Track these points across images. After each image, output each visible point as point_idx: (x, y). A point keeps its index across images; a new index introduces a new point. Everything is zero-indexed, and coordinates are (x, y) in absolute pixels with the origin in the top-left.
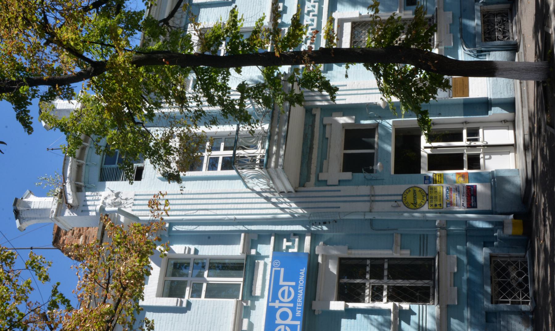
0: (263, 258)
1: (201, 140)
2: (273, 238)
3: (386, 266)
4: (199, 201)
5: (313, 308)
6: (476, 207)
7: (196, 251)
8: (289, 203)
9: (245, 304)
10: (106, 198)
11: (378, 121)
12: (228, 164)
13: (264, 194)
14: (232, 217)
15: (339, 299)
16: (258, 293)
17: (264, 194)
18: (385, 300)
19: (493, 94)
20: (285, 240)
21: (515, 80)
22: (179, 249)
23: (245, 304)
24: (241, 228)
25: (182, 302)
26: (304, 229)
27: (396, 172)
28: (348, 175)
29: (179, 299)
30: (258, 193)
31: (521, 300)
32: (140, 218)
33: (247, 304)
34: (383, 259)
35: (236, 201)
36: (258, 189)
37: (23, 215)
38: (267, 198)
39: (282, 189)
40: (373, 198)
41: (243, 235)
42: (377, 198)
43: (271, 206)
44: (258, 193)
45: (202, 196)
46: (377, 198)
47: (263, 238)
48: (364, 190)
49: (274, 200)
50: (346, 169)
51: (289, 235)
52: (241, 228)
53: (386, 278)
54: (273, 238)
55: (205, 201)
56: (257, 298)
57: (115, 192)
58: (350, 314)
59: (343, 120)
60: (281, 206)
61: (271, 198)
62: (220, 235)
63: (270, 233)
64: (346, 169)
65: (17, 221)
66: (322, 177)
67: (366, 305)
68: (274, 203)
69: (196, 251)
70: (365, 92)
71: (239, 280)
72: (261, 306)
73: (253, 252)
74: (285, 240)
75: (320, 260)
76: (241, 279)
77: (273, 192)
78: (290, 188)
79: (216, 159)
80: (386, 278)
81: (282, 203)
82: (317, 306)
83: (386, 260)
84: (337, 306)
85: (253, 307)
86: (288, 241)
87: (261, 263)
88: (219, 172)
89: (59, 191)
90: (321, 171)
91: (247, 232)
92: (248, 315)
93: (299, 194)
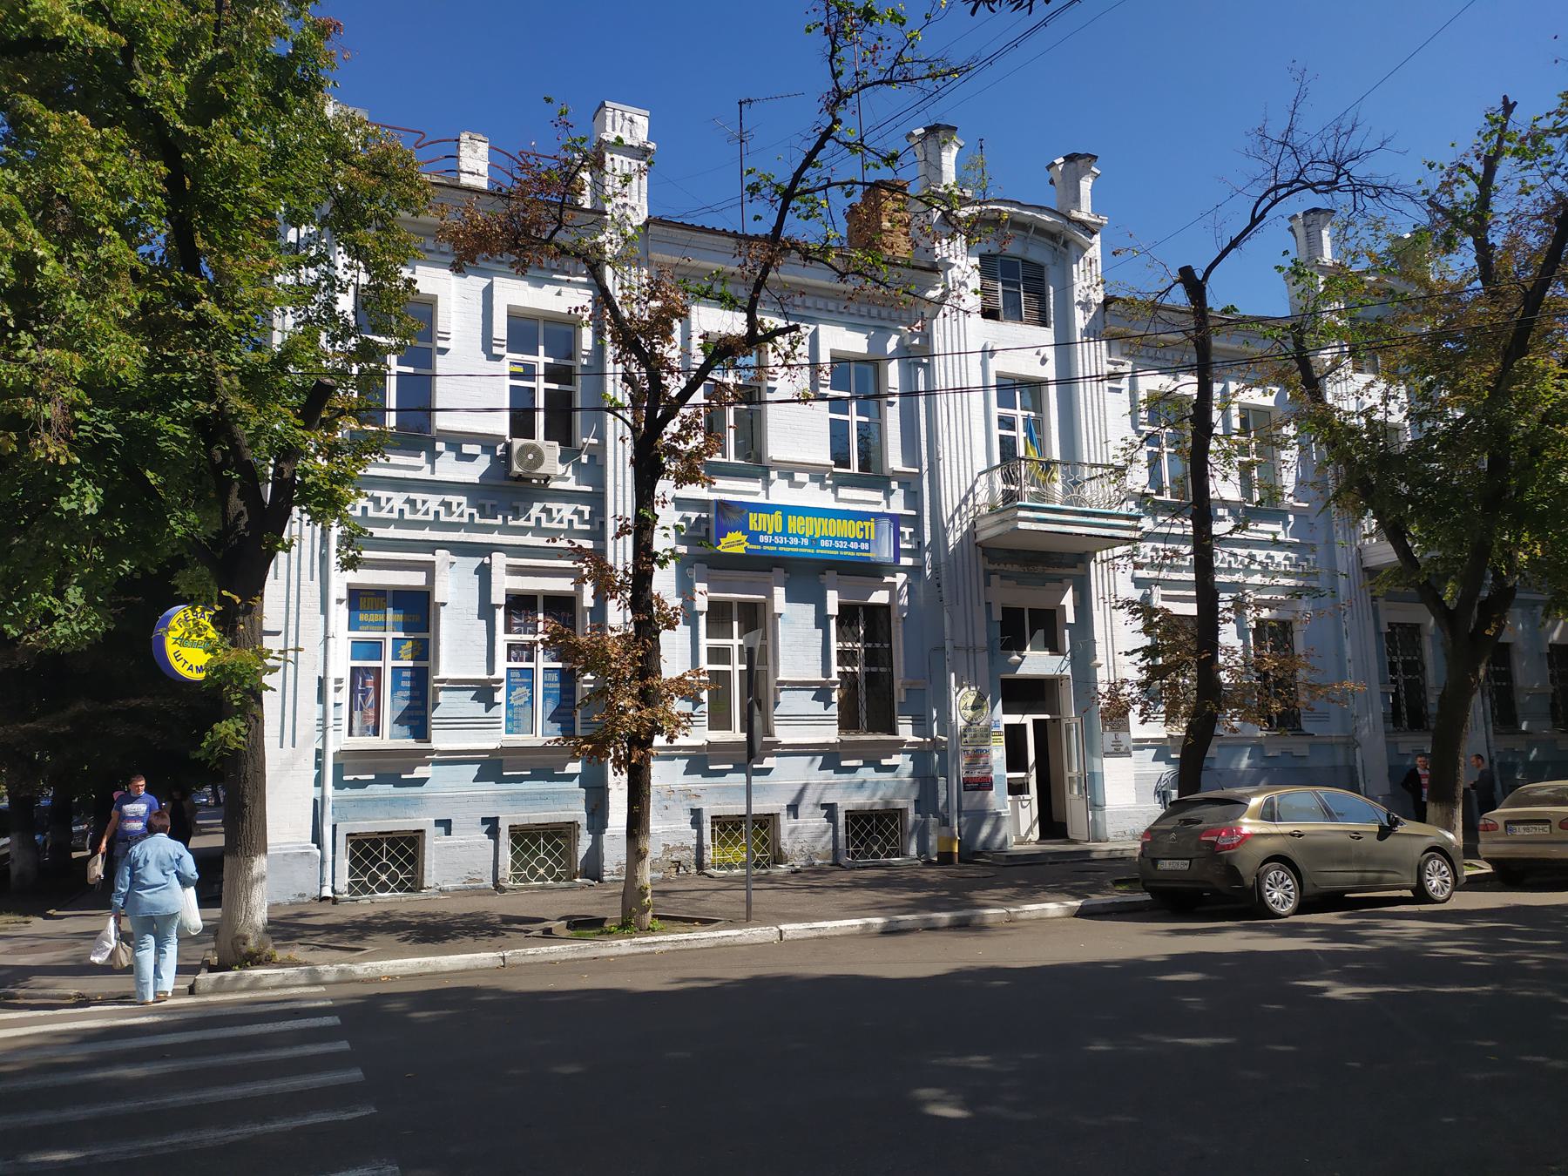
0: (887, 498)
1: (1037, 404)
2: (914, 513)
3: (882, 670)
4: (961, 465)
5: (827, 572)
6: (965, 790)
7: (892, 404)
8: (961, 529)
9: (827, 476)
10: (959, 267)
11: (1069, 655)
12: (1008, 445)
13: (971, 496)
14: (941, 456)
15: (841, 606)
16: (844, 492)
17: (971, 496)
18: (840, 669)
19: (1111, 814)
20: (912, 530)
21: (1213, 359)
22: (893, 375)
23: (827, 476)
24: (925, 467)
25: (826, 386)
26: (926, 543)
27: (1003, 680)
28: (998, 616)
29: (829, 383)
30: (972, 489)
31: (851, 849)
32: (935, 321)
33: (828, 479)
34: (891, 665)
35: (961, 460)
36: (978, 488)
37: (930, 141)
38: (965, 500)
39: (980, 524)
40: (971, 650)
41: (917, 470)
42: (971, 655)
43: (957, 504)
44: (972, 489)
45: (968, 448)
46: (971, 655)
47: (913, 498)
48: (982, 639)
49: (964, 509)
50: (1006, 611)
51: (917, 534)
52: (925, 467)
53: (868, 669)
54: (914, 513)
55: (960, 427)
56: (835, 492)
57: (967, 281)
58: (822, 621)
59: (1068, 600)
60: (957, 517)
61: (967, 505)
62: (914, 437)
63: (920, 510)
64: (1006, 611)
65: (922, 131)
66: (995, 579)
67: (835, 646)
68: (960, 507)
69: (892, 404)
70: (1109, 637)
71: (855, 468)
72: (825, 499)
73: (894, 485)
74: (912, 530)
75: (887, 579)
76: (856, 471)
77: (974, 509)
78: (982, 536)
79: (1012, 428)
80: (868, 669)
81: (960, 519)
82: (831, 575)
83: (886, 645)
84: (833, 601)
85: (824, 487)
86: (910, 533)
87: (881, 495)
88: (997, 432)
89: (967, 195)
90: (1002, 577)
91: (920, 475)
92: (813, 479)
93: (972, 547)
